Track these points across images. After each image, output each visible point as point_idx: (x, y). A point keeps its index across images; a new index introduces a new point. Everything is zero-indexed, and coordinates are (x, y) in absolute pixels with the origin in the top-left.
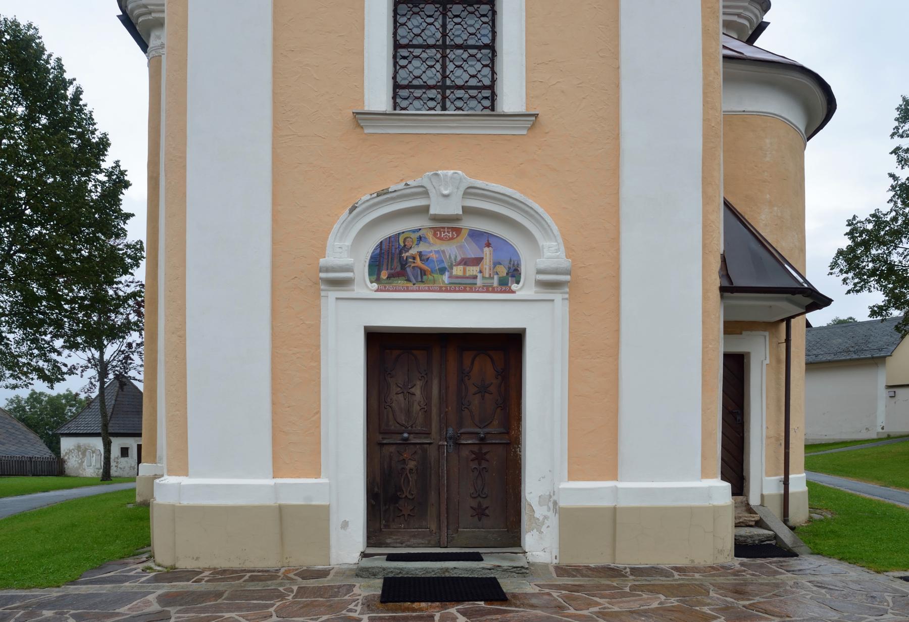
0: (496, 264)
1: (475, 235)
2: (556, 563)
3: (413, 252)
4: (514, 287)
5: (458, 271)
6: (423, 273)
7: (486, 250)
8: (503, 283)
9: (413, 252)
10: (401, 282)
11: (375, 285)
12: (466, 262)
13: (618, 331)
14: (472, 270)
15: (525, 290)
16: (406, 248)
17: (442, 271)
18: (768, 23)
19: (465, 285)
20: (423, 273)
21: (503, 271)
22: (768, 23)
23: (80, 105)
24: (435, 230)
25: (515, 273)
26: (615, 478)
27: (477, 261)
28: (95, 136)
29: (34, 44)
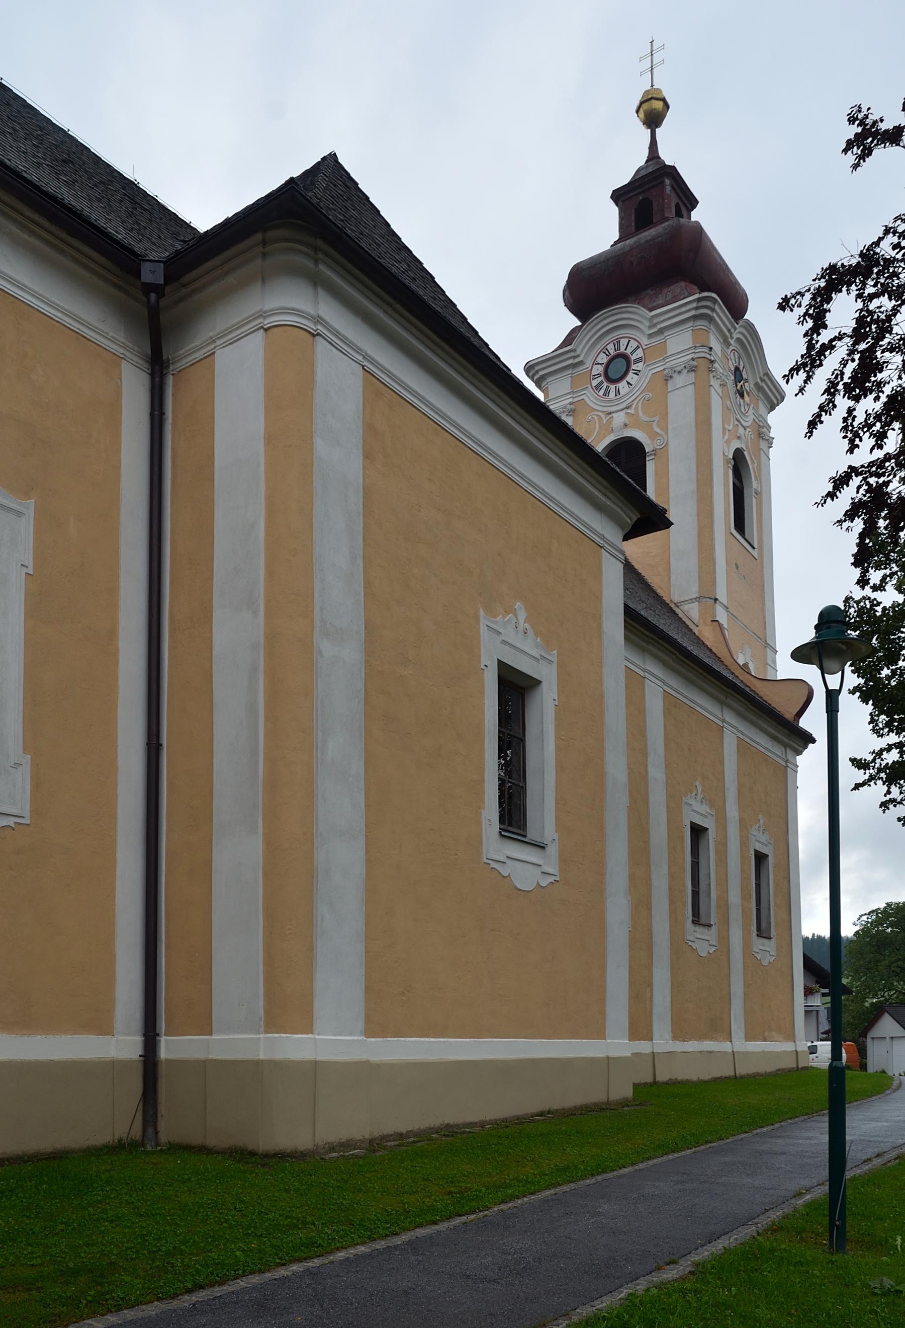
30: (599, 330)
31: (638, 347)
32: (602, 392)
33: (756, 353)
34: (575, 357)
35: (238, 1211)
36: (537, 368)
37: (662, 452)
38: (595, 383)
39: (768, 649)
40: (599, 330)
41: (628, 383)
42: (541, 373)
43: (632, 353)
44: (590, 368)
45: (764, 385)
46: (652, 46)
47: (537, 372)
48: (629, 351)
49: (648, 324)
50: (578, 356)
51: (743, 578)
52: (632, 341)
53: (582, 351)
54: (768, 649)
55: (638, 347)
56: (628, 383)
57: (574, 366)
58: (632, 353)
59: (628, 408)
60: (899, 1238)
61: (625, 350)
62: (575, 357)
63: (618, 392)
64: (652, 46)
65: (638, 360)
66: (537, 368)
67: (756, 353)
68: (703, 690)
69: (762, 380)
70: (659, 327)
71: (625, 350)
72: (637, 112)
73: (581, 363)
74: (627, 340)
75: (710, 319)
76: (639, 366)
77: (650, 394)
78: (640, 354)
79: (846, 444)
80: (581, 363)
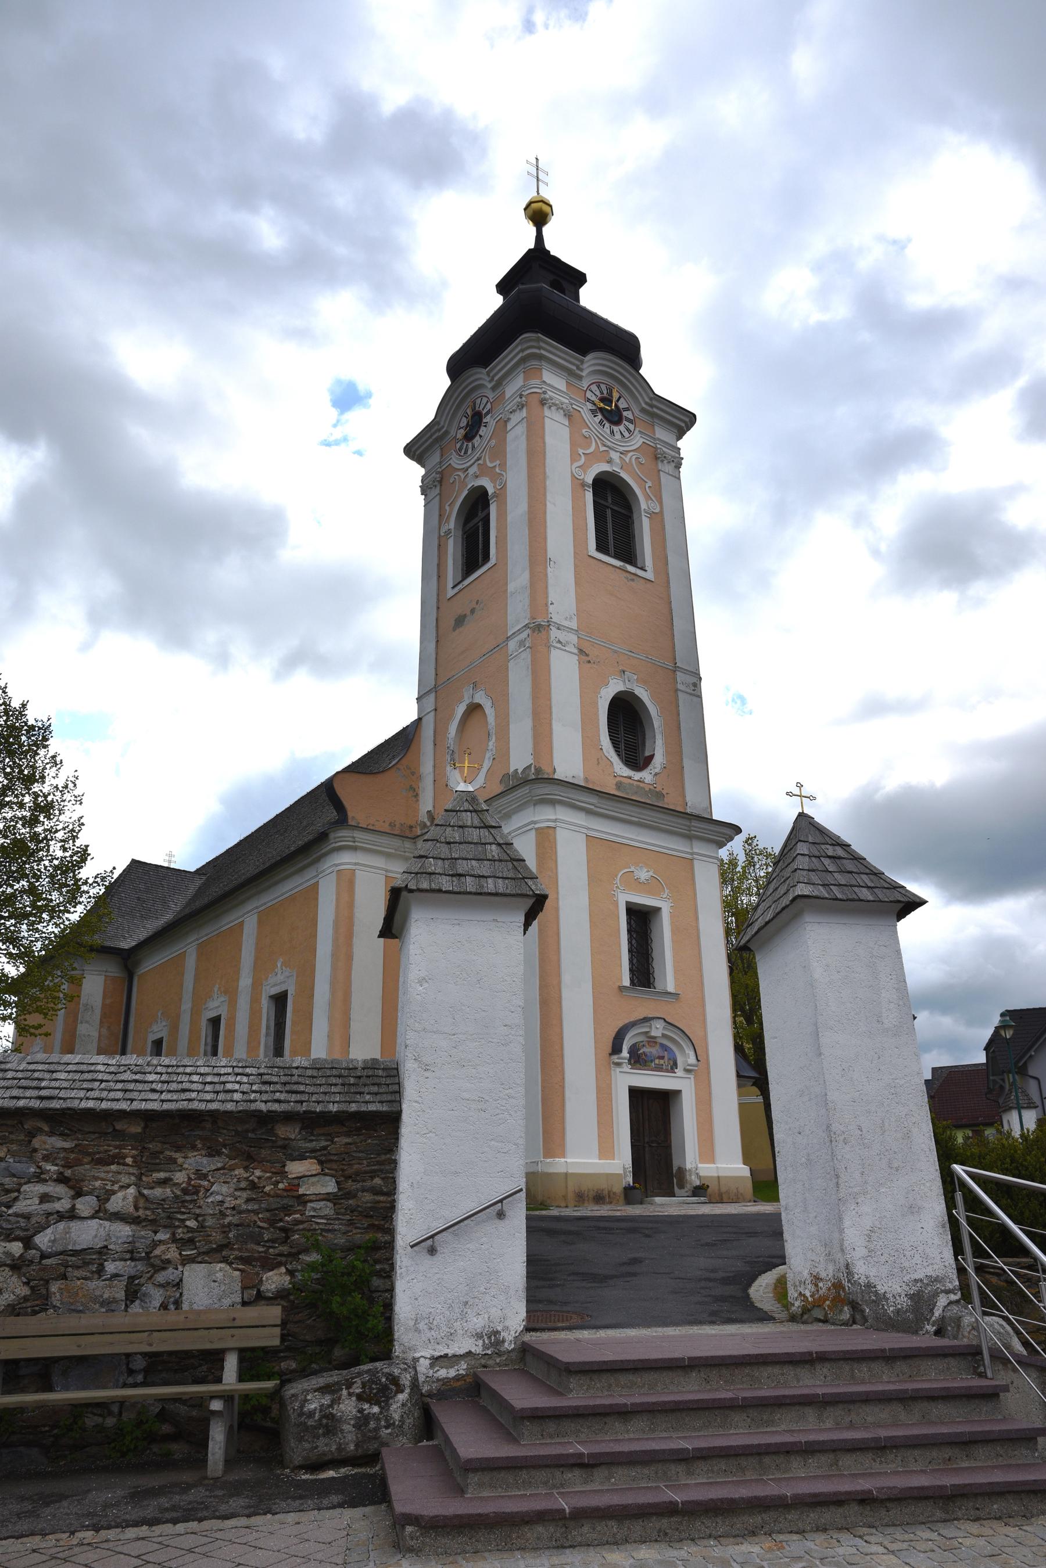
0: (669, 1059)
1: (662, 1046)
2: (742, 1544)
3: (641, 1051)
6: (646, 1061)
8: (672, 1068)
9: (641, 1051)
11: (630, 1066)
13: (710, 1093)
14: (662, 1062)
15: (679, 1072)
16: (639, 1050)
17: (652, 1061)
18: (379, 936)
19: (658, 1068)
20: (646, 1061)
21: (672, 1063)
22: (379, 936)
23: (276, 1136)
24: (648, 1042)
26: (564, 1157)
27: (662, 1058)
28: (180, 1268)
29: (14, 998)
33: (638, 386)
34: (439, 430)
35: (329, 1256)
36: (413, 449)
39: (678, 673)
40: (457, 398)
42: (543, 352)
45: (655, 410)
47: (539, 348)
49: (488, 379)
50: (443, 427)
54: (678, 673)
59: (479, 459)
62: (439, 430)
63: (473, 447)
66: (413, 449)
67: (638, 386)
68: (249, 898)
69: (652, 406)
70: (496, 378)
75: (541, 357)
76: (631, 427)
79: (334, 422)
80: (447, 433)
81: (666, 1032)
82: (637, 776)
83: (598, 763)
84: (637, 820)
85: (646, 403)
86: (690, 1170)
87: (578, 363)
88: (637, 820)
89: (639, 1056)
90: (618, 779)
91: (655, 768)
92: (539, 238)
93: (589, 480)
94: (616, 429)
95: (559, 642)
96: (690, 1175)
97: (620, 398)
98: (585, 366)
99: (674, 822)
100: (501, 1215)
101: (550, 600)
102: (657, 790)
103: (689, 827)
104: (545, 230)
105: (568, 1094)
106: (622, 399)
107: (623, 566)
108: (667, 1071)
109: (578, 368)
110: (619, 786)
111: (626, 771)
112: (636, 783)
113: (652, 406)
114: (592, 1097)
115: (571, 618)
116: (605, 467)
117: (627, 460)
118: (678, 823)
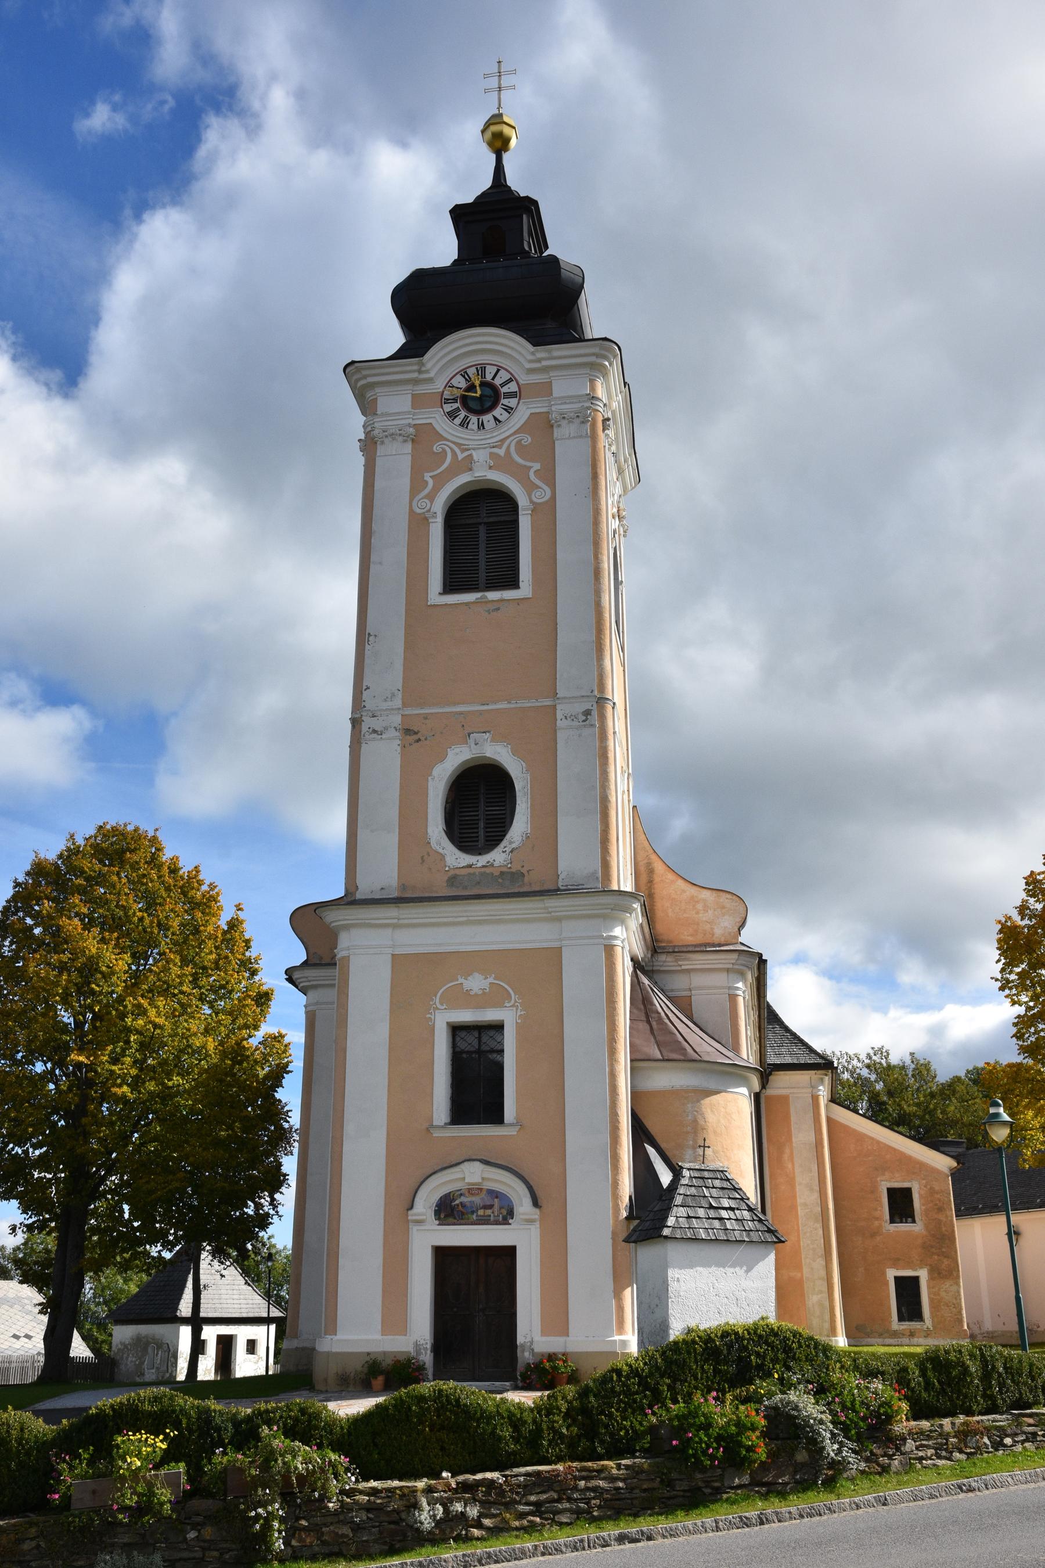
0: (501, 1208)
3: (457, 1202)
4: (510, 1221)
5: (481, 1212)
6: (463, 1214)
7: (496, 1200)
9: (457, 1202)
10: (451, 1220)
11: (437, 1222)
12: (486, 1207)
14: (489, 1212)
16: (454, 1200)
17: (473, 1212)
19: (484, 1221)
21: (505, 1212)
25: (511, 1213)
27: (491, 1207)
30: (449, 353)
31: (510, 381)
32: (458, 421)
37: (547, 512)
38: (448, 408)
40: (449, 353)
41: (496, 419)
42: (370, 380)
43: (503, 385)
44: (441, 390)
46: (499, 67)
47: (365, 377)
48: (498, 382)
51: (375, 735)
52: (502, 372)
53: (434, 365)
55: (510, 381)
56: (496, 419)
57: (416, 382)
58: (503, 385)
60: (126, 1207)
61: (493, 379)
64: (499, 67)
65: (511, 395)
69: (539, 360)
71: (493, 379)
72: (483, 132)
73: (430, 380)
74: (495, 369)
76: (512, 402)
77: (530, 439)
78: (512, 387)
81: (486, 1175)
82: (481, 860)
83: (423, 861)
84: (465, 919)
85: (530, 361)
86: (522, 1345)
87: (416, 367)
88: (465, 919)
89: (453, 1209)
90: (452, 873)
91: (511, 843)
92: (499, 171)
93: (439, 506)
94: (487, 418)
95: (375, 731)
96: (523, 1351)
97: (498, 371)
98: (429, 366)
99: (520, 909)
100: (1017, 1233)
101: (365, 684)
102: (513, 870)
103: (545, 908)
104: (506, 157)
105: (341, 1261)
106: (502, 372)
107: (481, 598)
108: (497, 1223)
109: (420, 372)
110: (453, 880)
111: (465, 859)
112: (479, 870)
113: (539, 360)
114: (375, 1262)
115: (393, 695)
116: (463, 479)
117: (501, 452)
118: (526, 909)
